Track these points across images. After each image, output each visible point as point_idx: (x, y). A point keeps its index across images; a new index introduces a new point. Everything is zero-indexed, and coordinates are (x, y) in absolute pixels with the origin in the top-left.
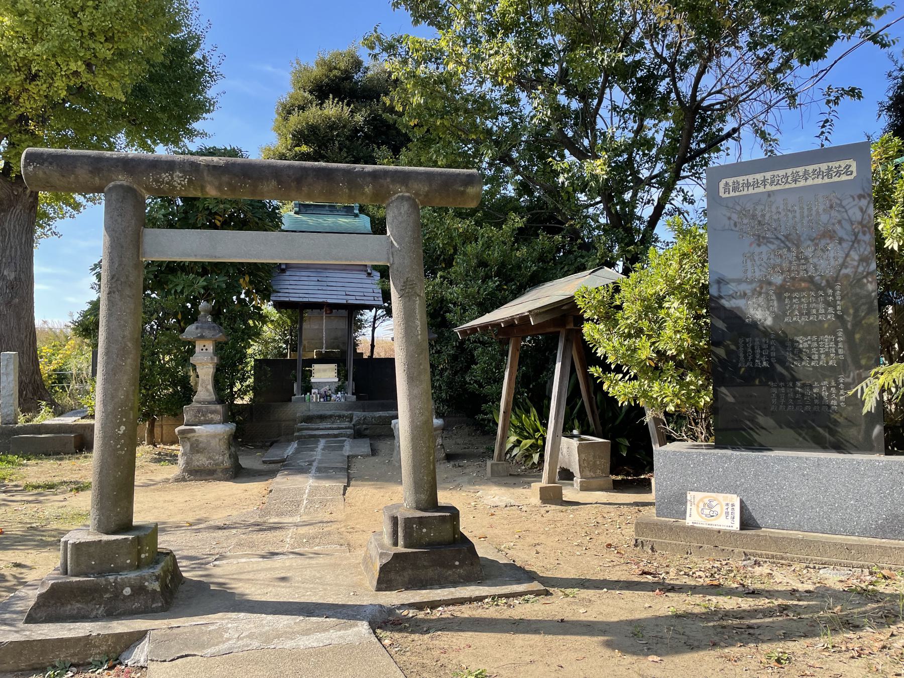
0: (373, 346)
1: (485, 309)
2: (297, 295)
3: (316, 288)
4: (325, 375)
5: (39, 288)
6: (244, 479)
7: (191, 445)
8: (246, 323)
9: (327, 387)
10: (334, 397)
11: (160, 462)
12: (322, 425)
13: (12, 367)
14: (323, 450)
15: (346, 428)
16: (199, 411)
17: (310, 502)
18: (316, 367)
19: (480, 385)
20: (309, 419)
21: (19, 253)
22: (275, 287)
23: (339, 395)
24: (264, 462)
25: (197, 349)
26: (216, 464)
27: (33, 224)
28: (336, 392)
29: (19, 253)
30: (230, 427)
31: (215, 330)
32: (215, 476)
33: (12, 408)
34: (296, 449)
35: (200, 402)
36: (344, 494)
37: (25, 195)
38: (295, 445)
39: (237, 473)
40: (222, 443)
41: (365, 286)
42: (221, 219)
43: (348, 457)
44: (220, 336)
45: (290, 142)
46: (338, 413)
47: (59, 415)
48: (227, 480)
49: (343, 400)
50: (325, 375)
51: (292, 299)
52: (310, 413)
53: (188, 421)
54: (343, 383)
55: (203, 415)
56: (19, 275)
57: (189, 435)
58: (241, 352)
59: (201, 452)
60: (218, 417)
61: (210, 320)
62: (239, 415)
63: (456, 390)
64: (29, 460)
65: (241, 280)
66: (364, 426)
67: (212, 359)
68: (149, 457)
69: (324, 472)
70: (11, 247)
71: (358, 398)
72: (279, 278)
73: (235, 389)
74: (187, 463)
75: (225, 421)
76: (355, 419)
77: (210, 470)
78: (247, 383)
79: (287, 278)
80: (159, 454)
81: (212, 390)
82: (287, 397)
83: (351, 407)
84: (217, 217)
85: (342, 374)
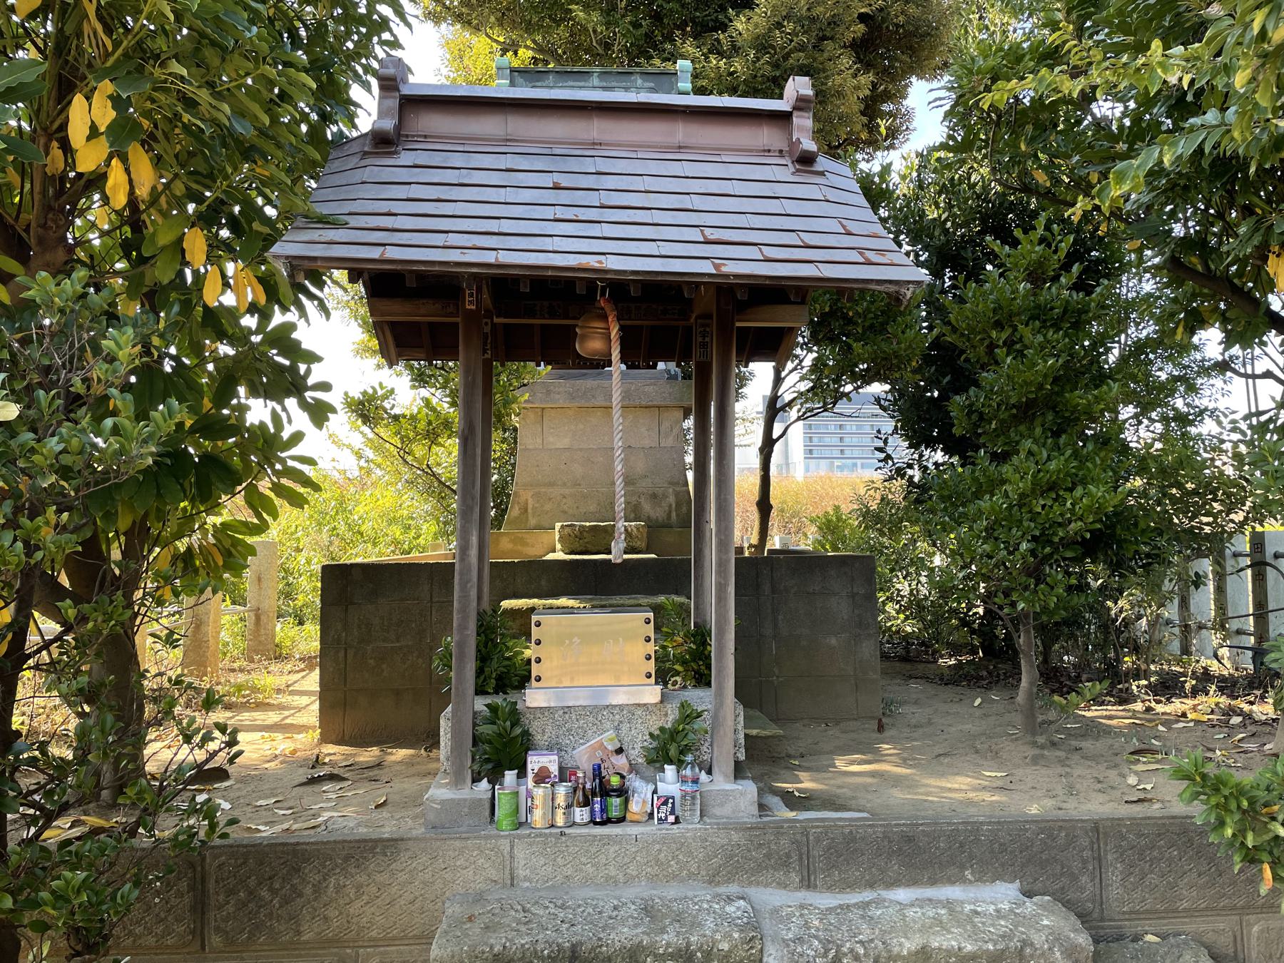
3: (549, 213)
9: (608, 739)
85: (684, 663)
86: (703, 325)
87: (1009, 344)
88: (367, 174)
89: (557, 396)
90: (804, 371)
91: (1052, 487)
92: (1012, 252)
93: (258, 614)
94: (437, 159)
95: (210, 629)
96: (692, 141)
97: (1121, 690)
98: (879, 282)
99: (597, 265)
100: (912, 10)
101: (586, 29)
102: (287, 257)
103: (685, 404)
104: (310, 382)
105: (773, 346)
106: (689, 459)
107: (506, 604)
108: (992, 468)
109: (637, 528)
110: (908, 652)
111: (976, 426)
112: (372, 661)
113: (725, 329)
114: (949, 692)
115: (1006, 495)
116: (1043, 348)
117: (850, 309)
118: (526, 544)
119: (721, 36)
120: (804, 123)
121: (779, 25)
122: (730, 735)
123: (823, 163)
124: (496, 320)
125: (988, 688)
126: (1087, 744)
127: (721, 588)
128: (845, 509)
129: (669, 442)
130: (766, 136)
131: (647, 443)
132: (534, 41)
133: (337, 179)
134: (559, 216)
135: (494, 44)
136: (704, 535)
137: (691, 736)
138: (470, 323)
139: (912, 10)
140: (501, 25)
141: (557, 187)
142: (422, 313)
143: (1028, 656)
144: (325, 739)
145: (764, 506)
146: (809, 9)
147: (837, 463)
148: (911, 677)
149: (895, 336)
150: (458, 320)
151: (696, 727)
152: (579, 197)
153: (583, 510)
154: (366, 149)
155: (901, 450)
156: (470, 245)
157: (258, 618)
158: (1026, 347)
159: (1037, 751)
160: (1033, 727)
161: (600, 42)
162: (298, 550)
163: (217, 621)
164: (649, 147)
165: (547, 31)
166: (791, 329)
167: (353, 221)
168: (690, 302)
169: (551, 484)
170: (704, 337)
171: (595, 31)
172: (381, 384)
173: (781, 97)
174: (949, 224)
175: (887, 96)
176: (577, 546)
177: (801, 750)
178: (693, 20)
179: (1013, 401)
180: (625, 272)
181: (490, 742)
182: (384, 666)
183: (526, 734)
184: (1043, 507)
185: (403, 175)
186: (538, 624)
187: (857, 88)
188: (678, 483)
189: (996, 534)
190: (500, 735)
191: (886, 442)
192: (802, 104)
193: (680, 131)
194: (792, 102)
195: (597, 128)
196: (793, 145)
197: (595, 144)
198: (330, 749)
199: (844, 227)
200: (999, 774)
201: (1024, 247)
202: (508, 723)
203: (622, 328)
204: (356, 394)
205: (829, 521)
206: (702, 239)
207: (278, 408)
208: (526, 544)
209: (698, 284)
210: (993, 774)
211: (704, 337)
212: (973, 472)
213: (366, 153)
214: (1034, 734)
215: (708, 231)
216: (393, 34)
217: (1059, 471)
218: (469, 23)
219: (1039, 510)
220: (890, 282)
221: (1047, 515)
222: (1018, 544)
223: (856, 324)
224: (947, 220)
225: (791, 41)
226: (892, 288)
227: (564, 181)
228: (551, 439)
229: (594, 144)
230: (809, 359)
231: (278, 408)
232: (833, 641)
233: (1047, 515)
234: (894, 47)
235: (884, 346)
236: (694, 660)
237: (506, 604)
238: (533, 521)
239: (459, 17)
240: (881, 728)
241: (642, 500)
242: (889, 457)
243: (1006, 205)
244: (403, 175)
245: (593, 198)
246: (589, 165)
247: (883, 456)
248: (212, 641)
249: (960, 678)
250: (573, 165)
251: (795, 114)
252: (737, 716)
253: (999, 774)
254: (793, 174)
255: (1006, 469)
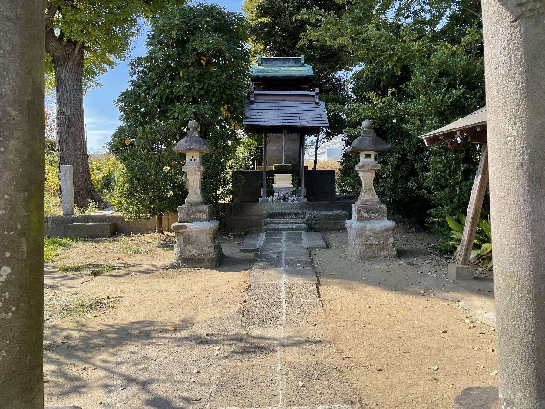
0: (316, 161)
1: (445, 120)
2: (263, 120)
3: (277, 115)
4: (283, 182)
5: (87, 121)
6: (227, 268)
7: (184, 239)
8: (225, 142)
9: (285, 192)
10: (290, 199)
11: (164, 247)
12: (283, 220)
13: (68, 175)
14: (286, 241)
15: (301, 223)
16: (189, 211)
17: (290, 305)
18: (277, 177)
19: (429, 191)
20: (272, 216)
21: (72, 96)
22: (247, 115)
23: (294, 197)
24: (242, 251)
25: (188, 159)
26: (204, 255)
27: (81, 75)
28: (292, 195)
29: (72, 96)
30: (214, 224)
31: (200, 143)
32: (203, 264)
33: (70, 204)
34: (265, 240)
35: (190, 203)
36: (319, 297)
37: (74, 54)
38: (263, 236)
39: (221, 262)
40: (208, 237)
41: (314, 112)
42: (205, 59)
43: (308, 249)
44: (205, 148)
45: (254, 14)
46: (294, 211)
47: (103, 209)
48: (212, 268)
49: (297, 202)
50: (283, 182)
51: (259, 123)
52: (273, 211)
53: (181, 218)
54: (297, 188)
55: (193, 214)
56: (73, 111)
57: (182, 231)
58: (222, 164)
59: (192, 245)
60: (205, 216)
61: (196, 135)
62: (222, 212)
63: (399, 195)
64: (77, 241)
65: (222, 109)
66: (314, 222)
67: (199, 167)
68: (158, 242)
69: (294, 267)
70: (67, 92)
71: (308, 200)
72: (250, 108)
73: (219, 193)
74: (181, 253)
75: (210, 219)
76: (307, 216)
77: (199, 260)
78: (227, 188)
79: (255, 108)
80: (165, 240)
81: (199, 194)
82: (256, 199)
83: (303, 207)
84: (203, 57)
85: (296, 182)
130: (311, 99)
167: (252, 117)
192: (317, 94)
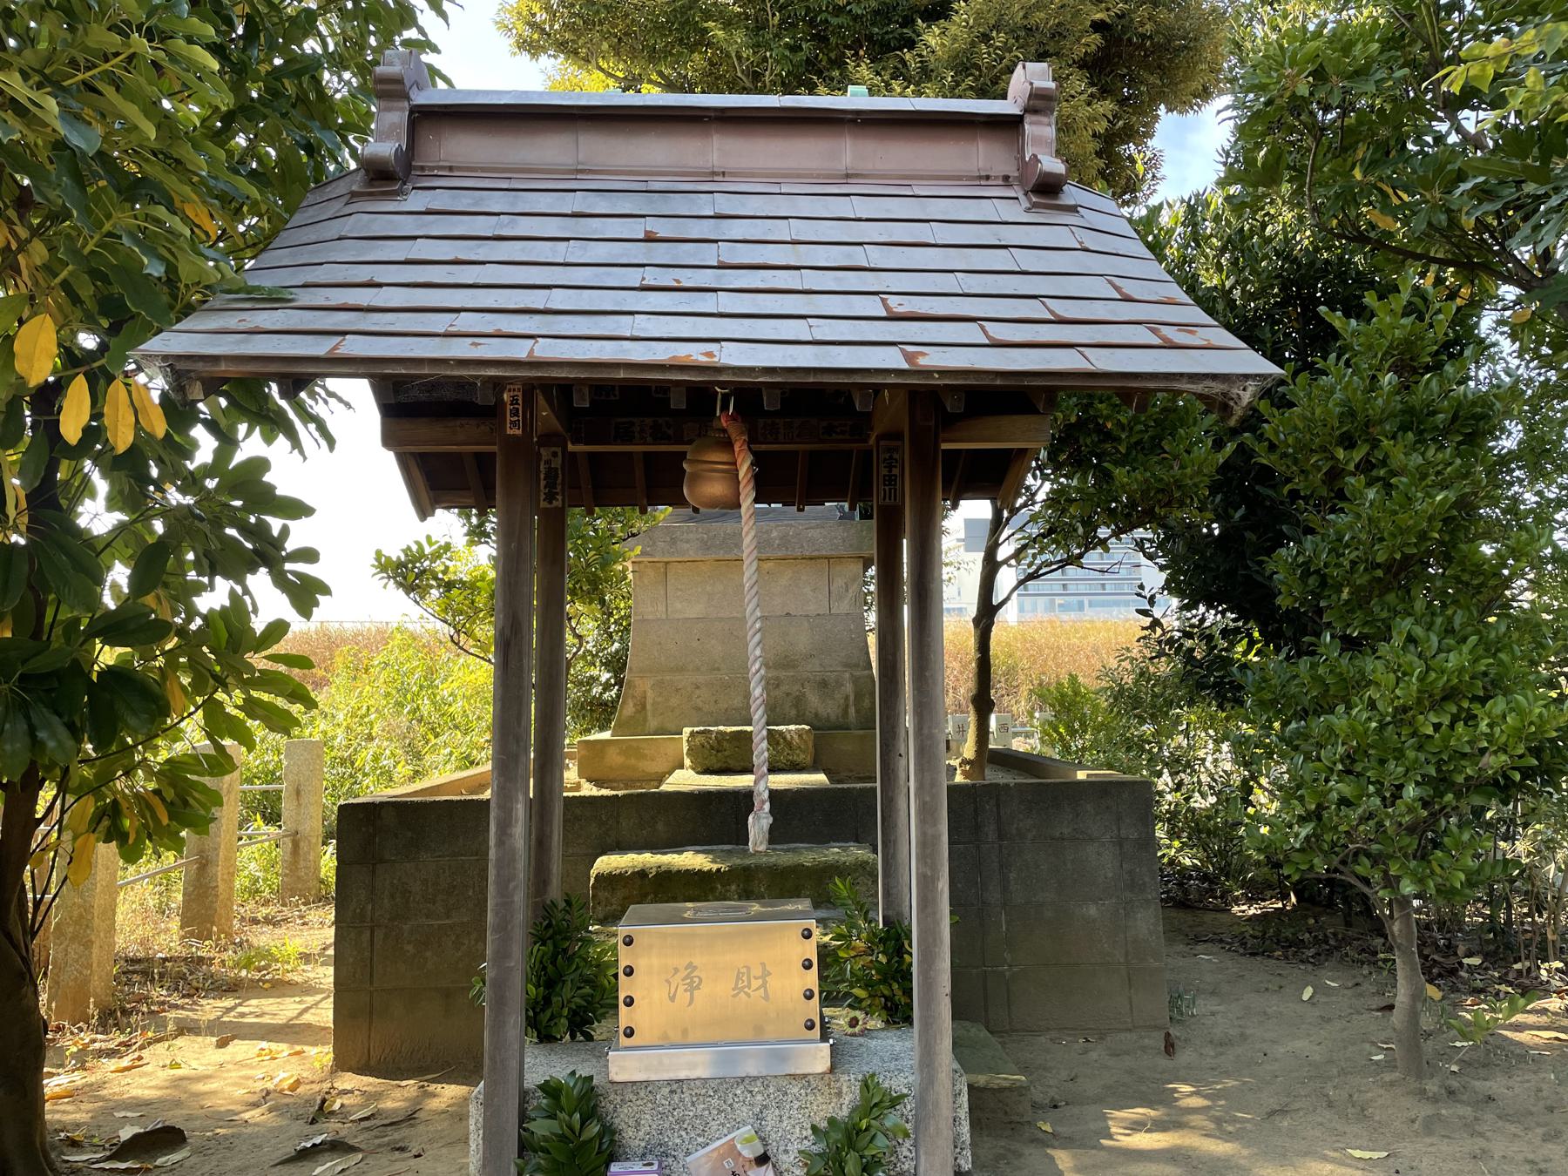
3: (633, 277)
85: (869, 982)
86: (889, 450)
87: (1366, 466)
88: (348, 226)
89: (686, 546)
90: (1037, 508)
91: (1450, 695)
92: (1362, 327)
93: (296, 839)
94: (464, 201)
95: (220, 871)
96: (867, 166)
97: (1519, 972)
98: (1194, 377)
99: (703, 359)
100: (1163, 15)
101: (728, 56)
102: (165, 358)
103: (866, 554)
104: (290, 546)
105: (992, 476)
106: (872, 618)
107: (608, 863)
108: (1344, 661)
109: (800, 733)
110: (1186, 892)
111: (1318, 596)
112: (409, 948)
113: (924, 457)
114: (1258, 971)
115: (1372, 705)
116: (1424, 477)
117: (1107, 418)
118: (644, 757)
119: (908, 57)
120: (1040, 131)
121: (985, 38)
122: (947, 1133)
123: (1071, 194)
124: (571, 447)
125: (1316, 962)
126: (1496, 1085)
127: (927, 883)
128: (1087, 682)
129: (843, 607)
130: (984, 154)
131: (812, 609)
132: (660, 74)
133: (309, 234)
134: (649, 282)
135: (611, 82)
136: (896, 777)
137: (881, 1141)
138: (540, 452)
139: (1163, 15)
140: (617, 54)
141: (650, 239)
142: (460, 439)
143: (1406, 953)
144: (342, 1063)
145: (983, 703)
146: (1025, 17)
147: (1059, 600)
148: (1197, 940)
149: (1176, 457)
150: (495, 448)
151: (888, 1124)
152: (685, 253)
153: (723, 705)
154: (354, 188)
155: (1169, 609)
156: (490, 330)
157: (296, 845)
158: (1393, 474)
159: (1426, 1110)
160: (1416, 1057)
161: (746, 73)
162: (370, 738)
163: (230, 860)
164: (799, 176)
165: (678, 60)
166: (1023, 452)
167: (306, 297)
168: (867, 417)
169: (681, 669)
170: (890, 467)
171: (739, 58)
172: (428, 538)
173: (1004, 97)
174: (1237, 293)
175: (1129, 134)
176: (714, 762)
177: (1052, 1093)
178: (870, 38)
179: (1381, 558)
180: (751, 370)
181: (545, 1151)
182: (428, 954)
183: (609, 1131)
184: (1437, 727)
185: (407, 225)
186: (629, 941)
187: (1092, 119)
188: (857, 665)
189: (1358, 768)
190: (563, 1138)
191: (1152, 601)
192: (1039, 103)
193: (848, 151)
194: (1022, 102)
195: (720, 149)
196: (1025, 166)
197: (713, 175)
198: (349, 1081)
199: (1052, 312)
200: (1375, 1155)
201: (1383, 318)
202: (577, 1116)
203: (759, 459)
204: (395, 553)
205: (1063, 695)
206: (884, 314)
207: (239, 589)
208: (644, 757)
209: (877, 388)
210: (1367, 1155)
211: (890, 467)
212: (1314, 666)
213: (354, 194)
214: (1419, 1076)
215: (893, 301)
216: (421, 31)
217: (1461, 670)
218: (576, 53)
219: (1430, 731)
220: (1214, 377)
221: (1446, 740)
222: (1400, 787)
223: (1118, 440)
224: (1233, 287)
225: (1002, 59)
226: (1217, 387)
227: (663, 229)
228: (679, 606)
229: (714, 173)
230: (1044, 490)
231: (239, 589)
232: (1093, 911)
233: (1446, 740)
234: (1135, 68)
235: (1159, 472)
236: (884, 981)
237: (608, 863)
238: (653, 723)
239: (562, 46)
240: (1170, 1047)
241: (807, 690)
242: (1156, 623)
243: (1318, 265)
244: (407, 225)
245: (709, 254)
246: (705, 205)
247: (1147, 621)
248: (222, 887)
249: (1267, 941)
250: (679, 205)
251: (1028, 119)
252: (956, 1095)
253: (1375, 1155)
254: (1027, 210)
255: (1370, 665)
